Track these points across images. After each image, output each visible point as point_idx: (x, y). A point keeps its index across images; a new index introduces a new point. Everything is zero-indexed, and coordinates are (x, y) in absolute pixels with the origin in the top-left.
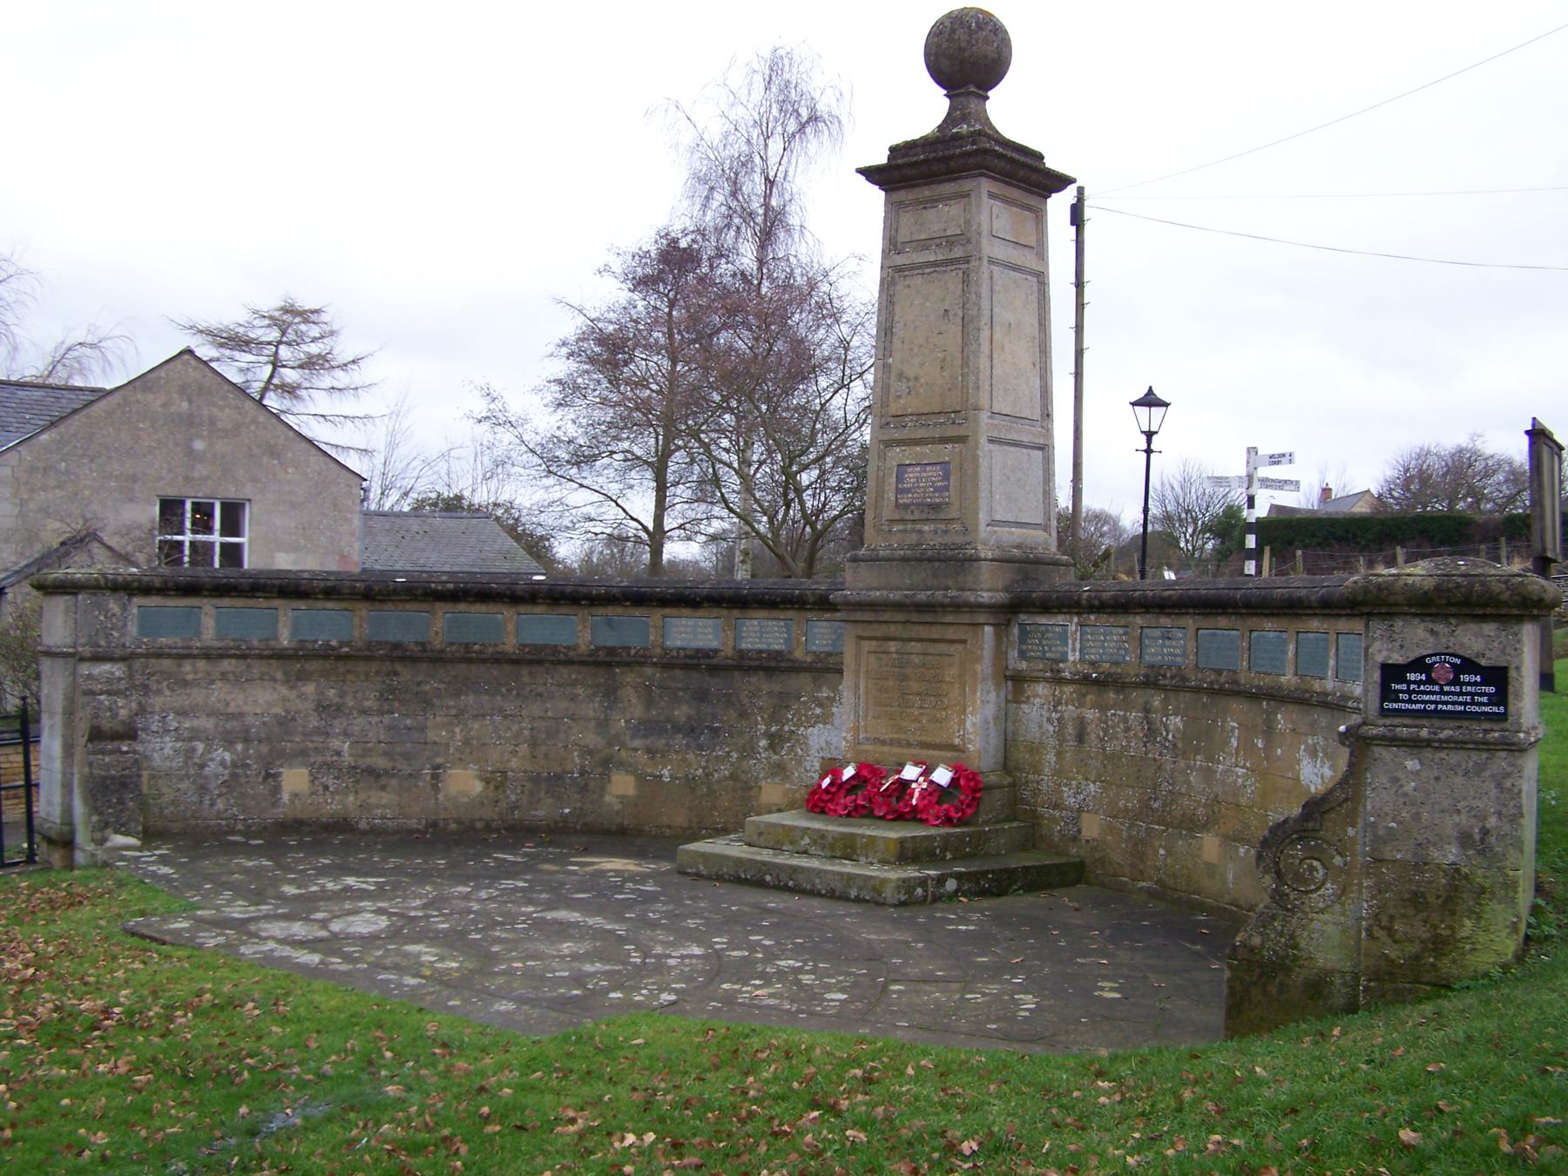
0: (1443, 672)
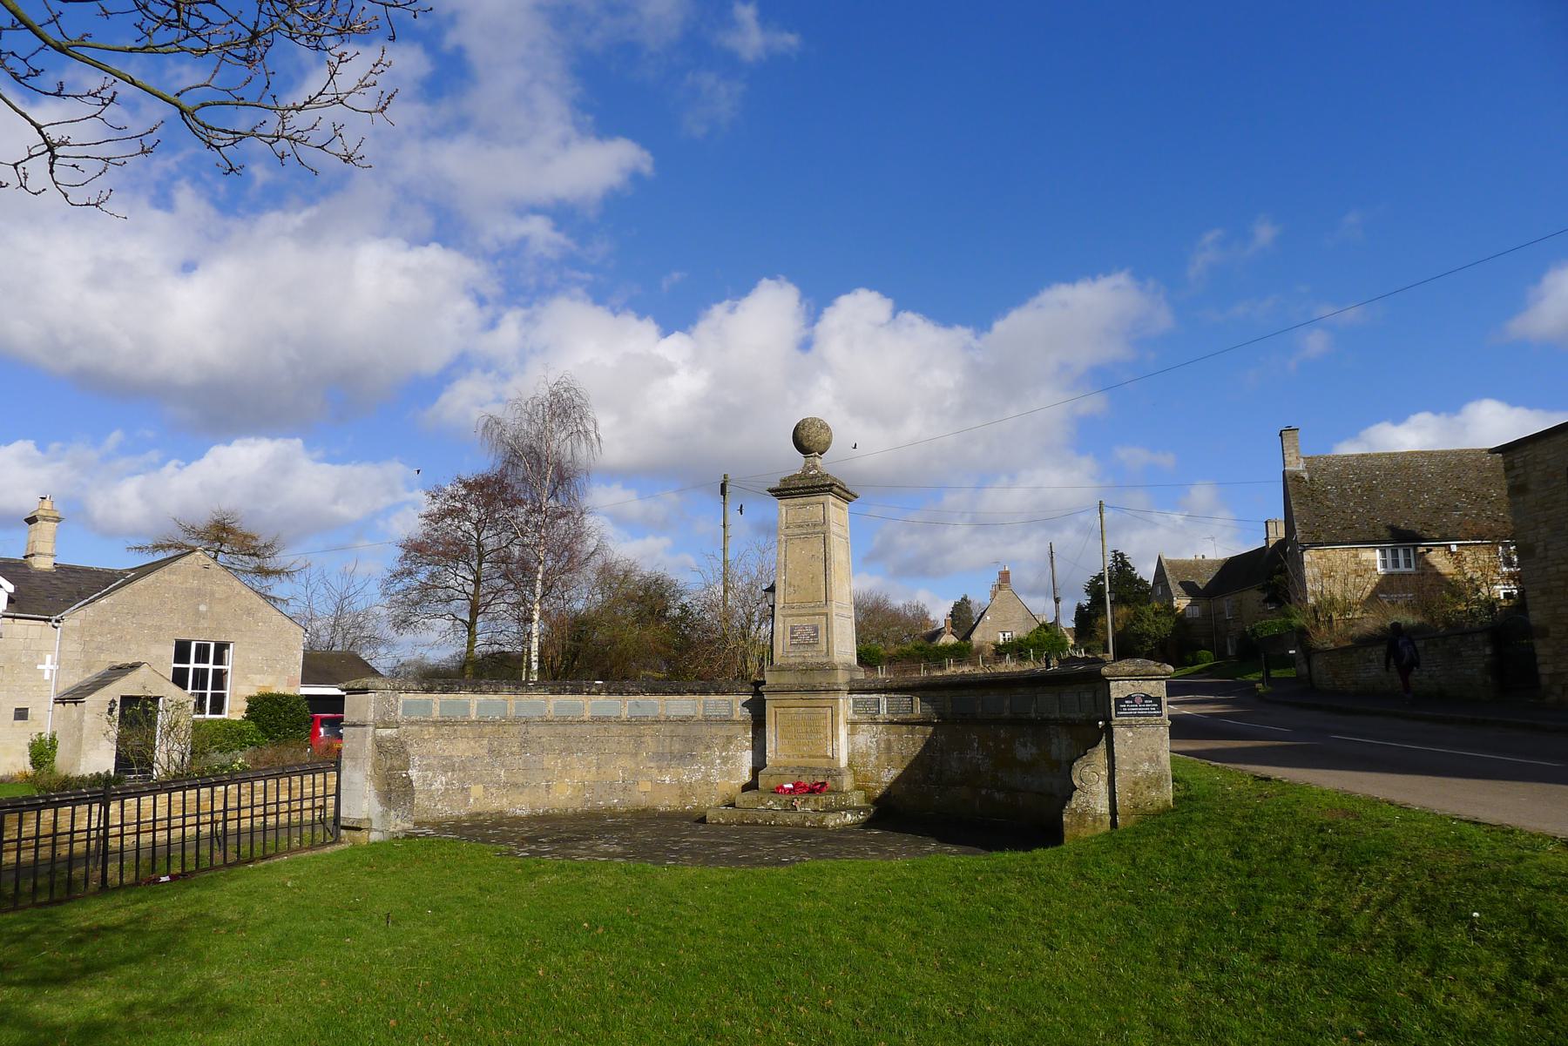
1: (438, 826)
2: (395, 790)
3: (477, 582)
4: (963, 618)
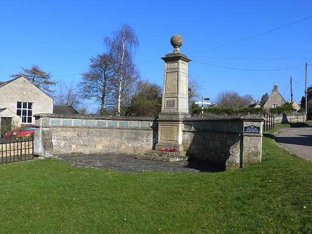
0: (252, 128)
1: (60, 156)
2: (47, 145)
3: (104, 87)
4: (265, 99)
